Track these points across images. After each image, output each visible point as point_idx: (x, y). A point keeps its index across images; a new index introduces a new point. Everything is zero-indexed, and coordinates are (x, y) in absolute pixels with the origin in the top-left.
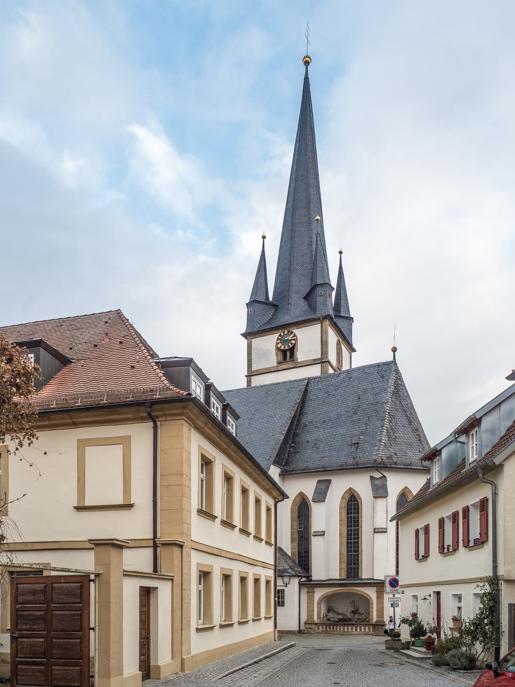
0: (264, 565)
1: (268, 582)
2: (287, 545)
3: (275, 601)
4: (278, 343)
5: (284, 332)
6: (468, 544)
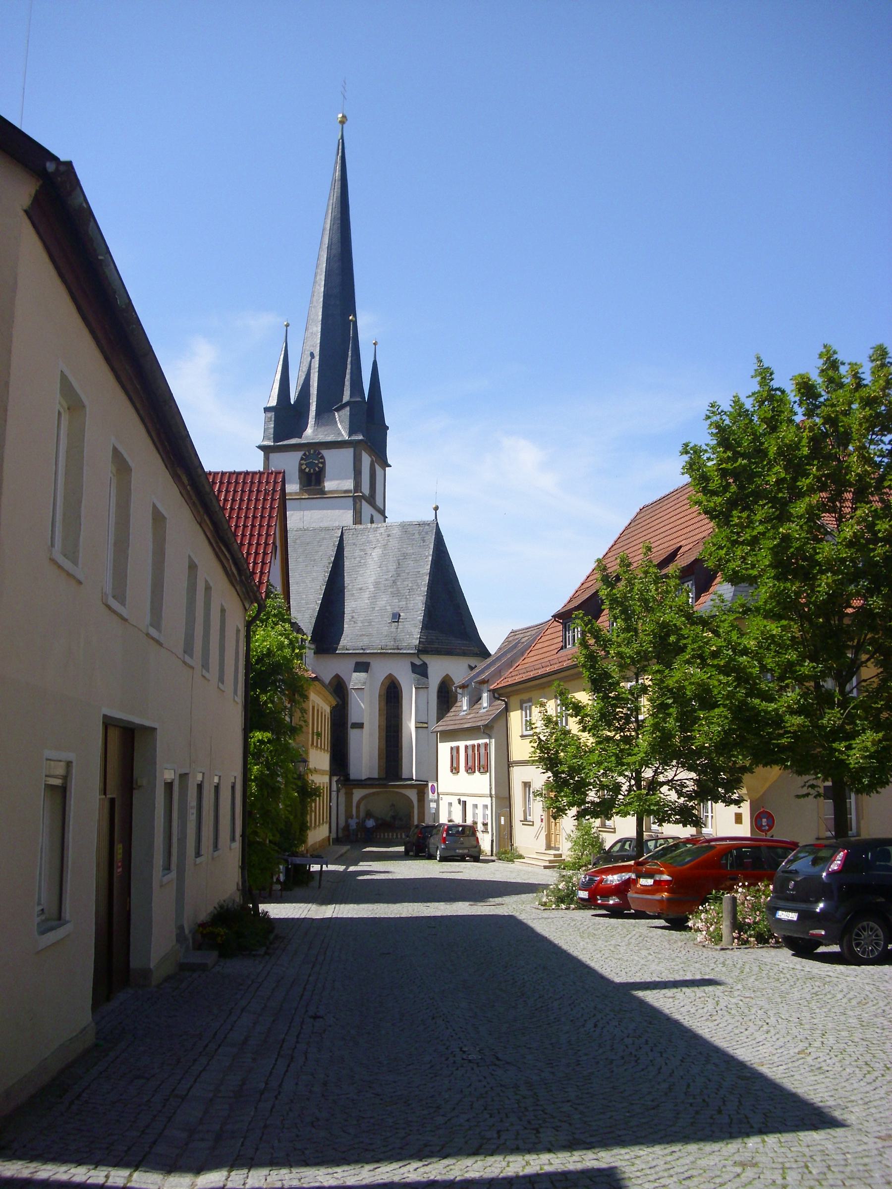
0: (322, 772)
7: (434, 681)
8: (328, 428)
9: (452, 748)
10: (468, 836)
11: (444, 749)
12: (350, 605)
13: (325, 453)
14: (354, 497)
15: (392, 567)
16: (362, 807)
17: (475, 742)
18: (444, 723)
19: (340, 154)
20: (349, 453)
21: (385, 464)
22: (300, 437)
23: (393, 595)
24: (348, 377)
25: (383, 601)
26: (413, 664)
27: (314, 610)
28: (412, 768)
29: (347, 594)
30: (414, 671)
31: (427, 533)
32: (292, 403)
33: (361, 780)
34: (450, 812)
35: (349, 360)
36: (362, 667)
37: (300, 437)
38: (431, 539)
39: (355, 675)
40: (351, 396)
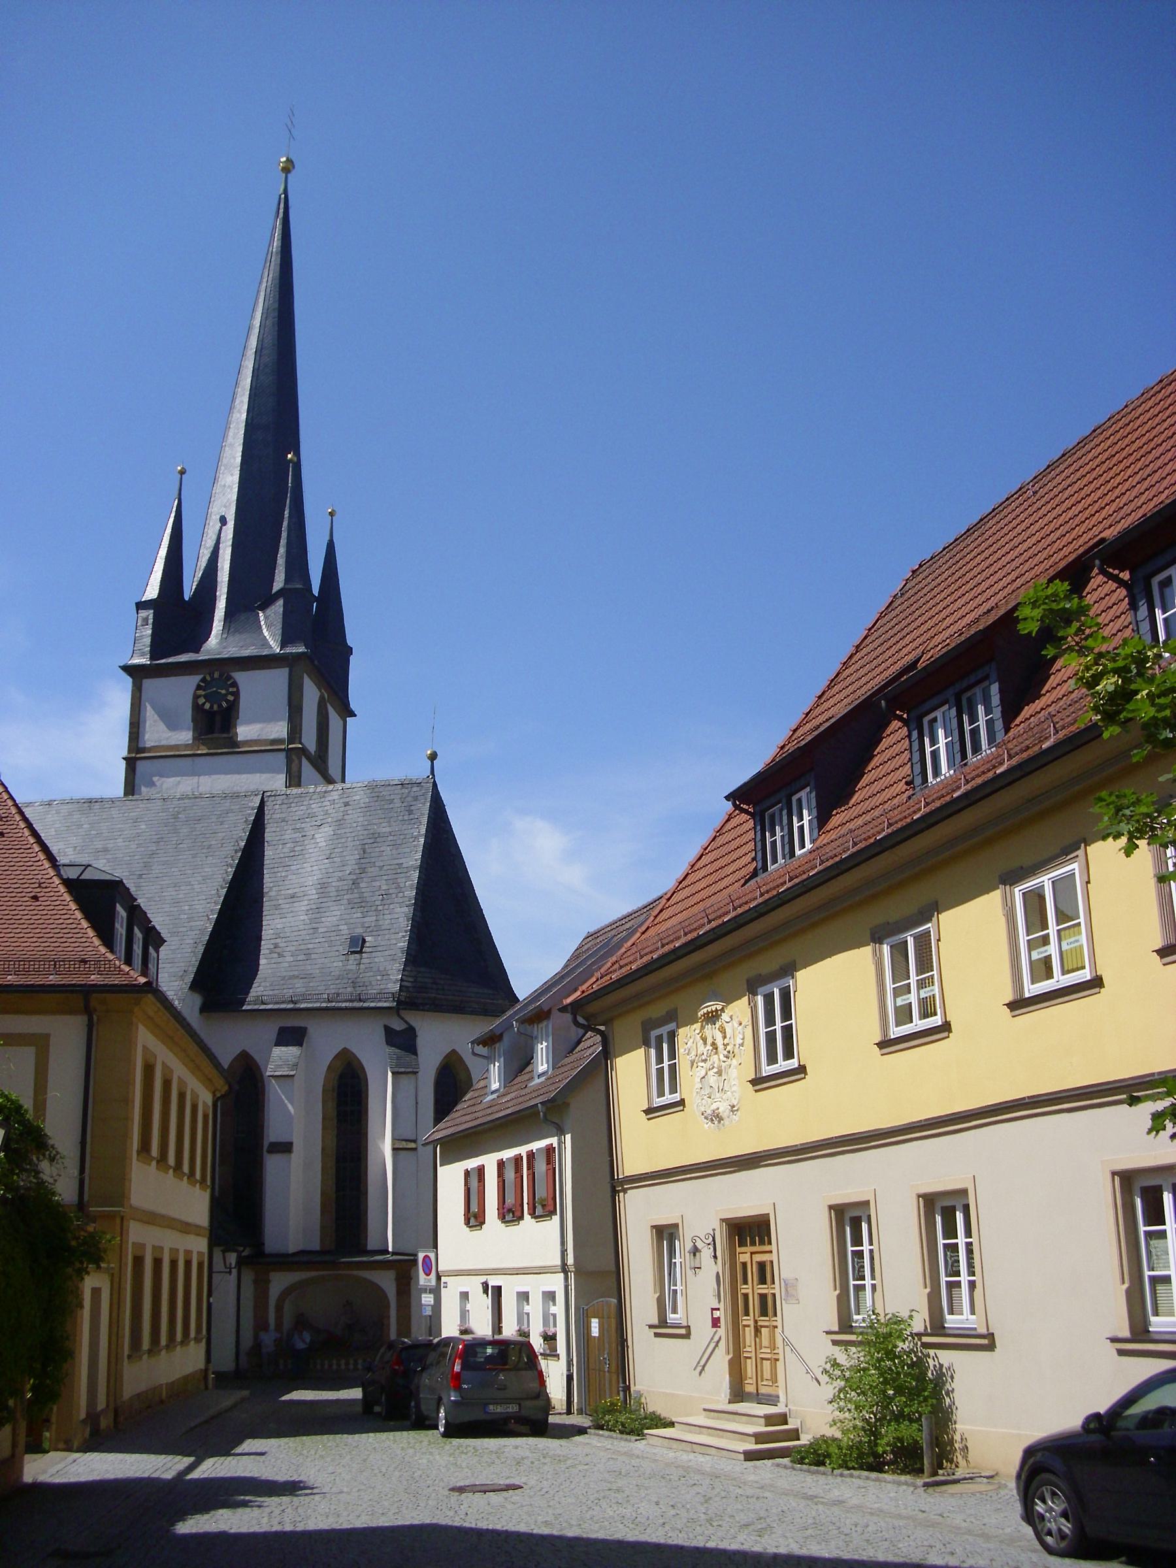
0: (186, 1228)
4: (199, 696)
5: (211, 674)
7: (430, 1059)
8: (244, 636)
9: (467, 1173)
10: (516, 1368)
11: (451, 1179)
12: (272, 925)
13: (241, 677)
15: (352, 858)
16: (287, 1307)
17: (523, 1150)
18: (449, 1124)
19: (281, 215)
20: (279, 678)
21: (347, 712)
22: (197, 651)
24: (282, 550)
25: (334, 915)
26: (388, 1029)
28: (387, 1232)
29: (267, 905)
31: (416, 799)
32: (187, 599)
33: (288, 1255)
34: (464, 1314)
35: (285, 524)
36: (292, 1036)
37: (197, 651)
39: (278, 1051)
40: (287, 581)
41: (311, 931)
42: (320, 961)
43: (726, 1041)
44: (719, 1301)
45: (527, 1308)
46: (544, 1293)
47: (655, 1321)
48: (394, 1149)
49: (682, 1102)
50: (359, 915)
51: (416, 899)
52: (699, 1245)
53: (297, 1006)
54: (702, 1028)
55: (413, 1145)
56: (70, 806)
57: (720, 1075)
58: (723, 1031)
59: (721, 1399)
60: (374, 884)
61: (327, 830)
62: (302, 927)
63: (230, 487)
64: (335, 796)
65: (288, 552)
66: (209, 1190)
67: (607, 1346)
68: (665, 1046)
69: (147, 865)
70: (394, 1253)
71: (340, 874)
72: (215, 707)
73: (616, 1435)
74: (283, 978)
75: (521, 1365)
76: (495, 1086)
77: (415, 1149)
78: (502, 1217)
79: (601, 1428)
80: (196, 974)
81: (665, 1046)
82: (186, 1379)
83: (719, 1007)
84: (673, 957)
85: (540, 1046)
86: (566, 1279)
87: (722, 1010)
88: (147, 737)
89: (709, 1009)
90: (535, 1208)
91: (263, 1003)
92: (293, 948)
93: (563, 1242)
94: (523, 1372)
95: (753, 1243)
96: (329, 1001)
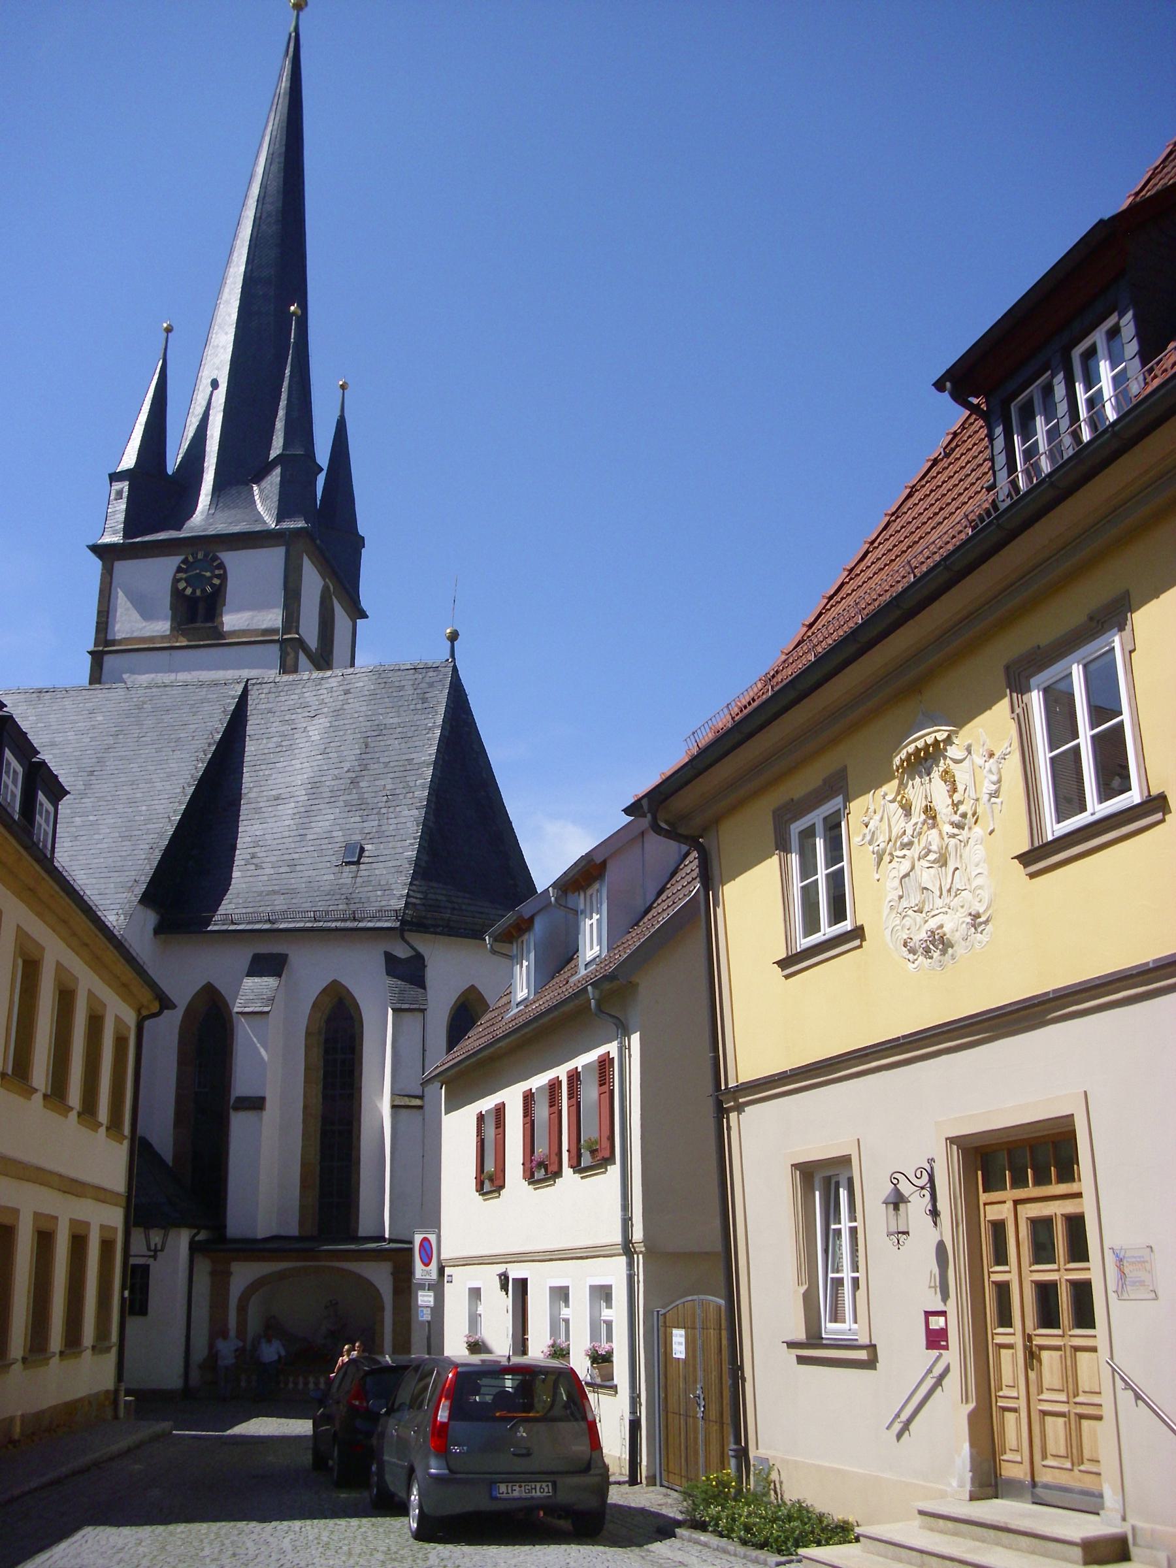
0: (100, 1194)
1: (107, 1246)
2: (162, 1134)
3: (123, 1298)
4: (179, 580)
5: (194, 555)
6: (579, 1163)
7: (441, 996)
8: (233, 512)
9: (481, 1118)
11: (458, 1130)
13: (229, 558)
14: (282, 642)
15: (351, 753)
17: (561, 1072)
20: (273, 559)
23: (350, 807)
24: (281, 413)
26: (390, 959)
27: (161, 835)
28: (381, 1212)
30: (390, 972)
31: (431, 685)
33: (256, 1241)
34: (474, 1320)
35: (286, 384)
36: (268, 965)
38: (441, 697)
39: (250, 983)
41: (298, 838)
42: (307, 874)
43: (957, 797)
44: (945, 1297)
45: (565, 1312)
46: (592, 1288)
47: (801, 1336)
48: (393, 1107)
49: (858, 933)
50: (358, 819)
51: (428, 800)
52: (905, 1188)
53: (275, 926)
54: (902, 785)
55: (418, 1102)
56: (16, 697)
57: (945, 864)
58: (949, 779)
59: (952, 1487)
60: (377, 783)
61: (322, 722)
62: (287, 834)
63: (224, 348)
64: (333, 682)
65: (287, 414)
66: (126, 1143)
67: (700, 1374)
68: (820, 844)
69: (100, 761)
70: (391, 1241)
71: (336, 772)
72: (198, 593)
73: (733, 1546)
74: (260, 894)
75: (557, 1411)
76: (521, 993)
77: (421, 1107)
78: (530, 1177)
79: (701, 1526)
80: (151, 883)
81: (820, 844)
82: (89, 1400)
83: (941, 736)
84: (852, 649)
85: (588, 922)
86: (630, 1265)
87: (948, 741)
88: (117, 627)
89: (920, 744)
90: (579, 1156)
91: (233, 923)
92: (274, 859)
93: (626, 1206)
94: (561, 1425)
95: (1019, 1181)
96: (316, 920)
